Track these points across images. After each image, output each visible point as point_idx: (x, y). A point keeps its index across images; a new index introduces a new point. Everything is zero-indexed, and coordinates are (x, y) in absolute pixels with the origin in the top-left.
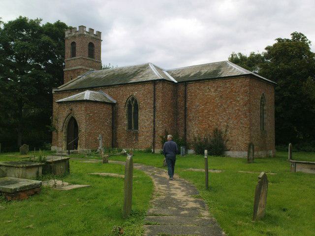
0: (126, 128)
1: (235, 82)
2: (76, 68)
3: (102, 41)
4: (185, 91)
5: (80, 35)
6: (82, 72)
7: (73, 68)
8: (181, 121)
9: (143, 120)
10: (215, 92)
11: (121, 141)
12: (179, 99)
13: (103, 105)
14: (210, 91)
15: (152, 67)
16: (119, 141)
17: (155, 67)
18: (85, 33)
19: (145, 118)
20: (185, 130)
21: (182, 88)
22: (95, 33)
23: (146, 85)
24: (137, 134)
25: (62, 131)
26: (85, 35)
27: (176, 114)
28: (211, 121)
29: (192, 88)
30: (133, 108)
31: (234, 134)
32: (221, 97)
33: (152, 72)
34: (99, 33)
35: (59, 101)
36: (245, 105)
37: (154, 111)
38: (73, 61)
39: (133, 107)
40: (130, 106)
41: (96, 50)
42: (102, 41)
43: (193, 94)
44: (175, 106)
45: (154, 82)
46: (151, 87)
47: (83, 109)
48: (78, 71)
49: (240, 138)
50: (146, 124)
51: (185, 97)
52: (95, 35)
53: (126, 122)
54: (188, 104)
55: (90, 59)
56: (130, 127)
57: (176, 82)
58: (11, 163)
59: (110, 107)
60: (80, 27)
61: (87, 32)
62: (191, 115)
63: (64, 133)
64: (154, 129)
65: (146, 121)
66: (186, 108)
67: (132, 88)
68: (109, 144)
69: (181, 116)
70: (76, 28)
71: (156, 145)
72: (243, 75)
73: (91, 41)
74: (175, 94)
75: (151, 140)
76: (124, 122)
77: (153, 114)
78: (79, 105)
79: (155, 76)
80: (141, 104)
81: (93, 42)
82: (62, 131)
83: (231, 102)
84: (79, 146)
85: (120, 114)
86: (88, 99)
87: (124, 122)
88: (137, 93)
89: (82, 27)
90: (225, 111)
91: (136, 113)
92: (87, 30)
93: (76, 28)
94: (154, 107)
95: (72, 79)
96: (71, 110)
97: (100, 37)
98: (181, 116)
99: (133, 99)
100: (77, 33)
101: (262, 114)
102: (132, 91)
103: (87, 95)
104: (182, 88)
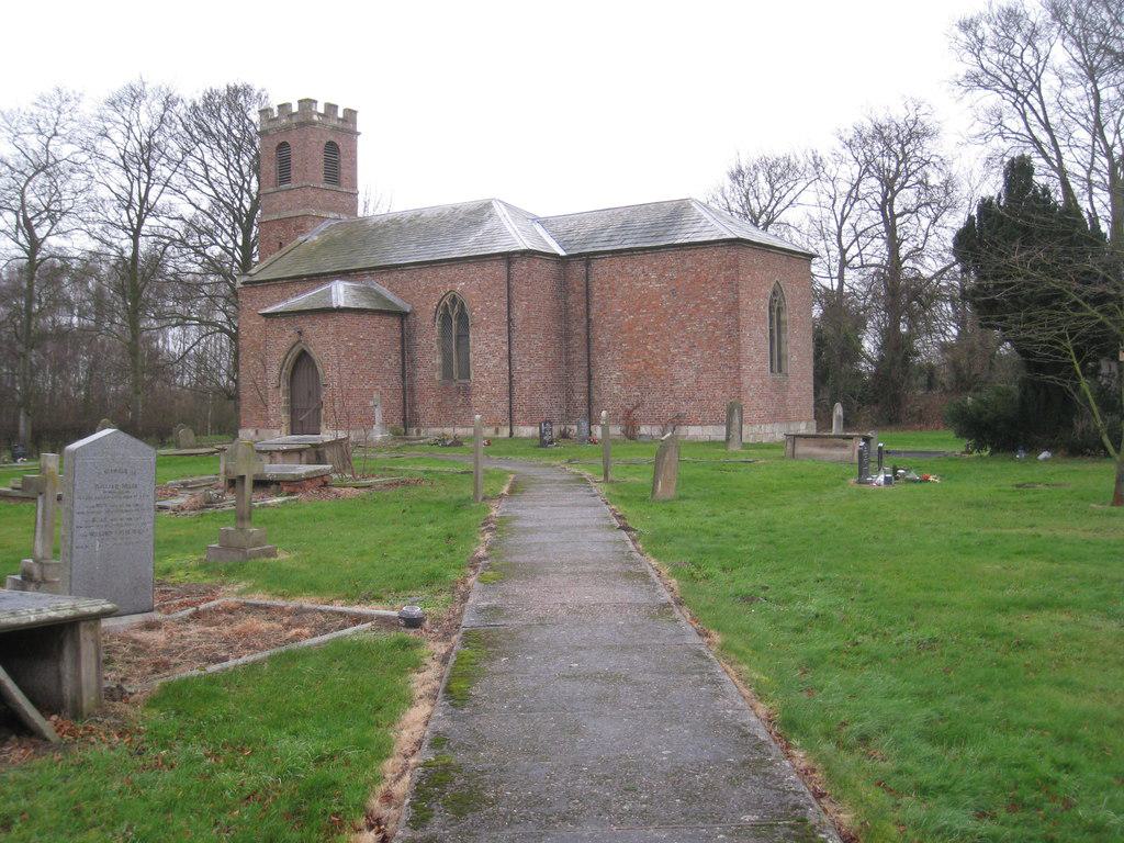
0: (437, 376)
1: (705, 257)
2: (292, 214)
3: (359, 134)
4: (587, 275)
5: (301, 125)
6: (309, 224)
7: (285, 215)
8: (580, 355)
9: (481, 355)
10: (658, 281)
11: (427, 407)
12: (571, 298)
13: (377, 318)
14: (649, 279)
15: (499, 210)
16: (420, 409)
17: (506, 205)
18: (315, 118)
19: (485, 349)
20: (590, 378)
21: (578, 269)
22: (340, 114)
23: (488, 264)
24: (466, 391)
25: (278, 387)
26: (314, 123)
27: (566, 336)
28: (651, 353)
29: (601, 269)
30: (454, 322)
31: (704, 383)
32: (673, 292)
33: (503, 233)
34: (351, 115)
35: (267, 311)
36: (998, 394)
37: (509, 331)
38: (283, 196)
39: (455, 319)
40: (446, 319)
41: (344, 162)
42: (359, 134)
43: (607, 286)
44: (563, 315)
45: (509, 258)
46: (500, 270)
47: (331, 329)
48: (299, 222)
49: (719, 392)
50: (490, 365)
51: (588, 293)
52: (339, 119)
53: (438, 361)
54: (593, 311)
55: (328, 186)
56: (447, 374)
57: (562, 253)
58: (845, 446)
59: (394, 322)
60: (300, 102)
61: (319, 114)
62: (602, 338)
63: (283, 391)
64: (511, 377)
65: (488, 356)
66: (589, 321)
67: (452, 272)
68: (397, 422)
69: (577, 342)
70: (290, 105)
71: (518, 416)
72: (724, 241)
73: (331, 138)
74: (563, 285)
75: (504, 406)
76: (430, 360)
77: (506, 340)
78: (319, 321)
79: (507, 241)
80: (475, 313)
81: (337, 141)
82: (278, 387)
83: (697, 305)
84: (323, 427)
85: (421, 341)
86: (342, 305)
87: (430, 360)
88: (464, 285)
89: (307, 104)
90: (684, 327)
91: (463, 337)
92: (321, 109)
93: (290, 105)
94: (510, 320)
95: (281, 245)
96: (300, 333)
97: (355, 123)
98: (577, 342)
99: (454, 300)
100: (295, 120)
101: (776, 335)
102: (452, 281)
103: (341, 293)
104: (578, 269)
